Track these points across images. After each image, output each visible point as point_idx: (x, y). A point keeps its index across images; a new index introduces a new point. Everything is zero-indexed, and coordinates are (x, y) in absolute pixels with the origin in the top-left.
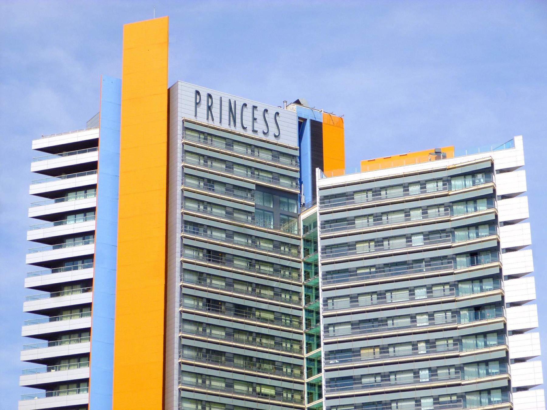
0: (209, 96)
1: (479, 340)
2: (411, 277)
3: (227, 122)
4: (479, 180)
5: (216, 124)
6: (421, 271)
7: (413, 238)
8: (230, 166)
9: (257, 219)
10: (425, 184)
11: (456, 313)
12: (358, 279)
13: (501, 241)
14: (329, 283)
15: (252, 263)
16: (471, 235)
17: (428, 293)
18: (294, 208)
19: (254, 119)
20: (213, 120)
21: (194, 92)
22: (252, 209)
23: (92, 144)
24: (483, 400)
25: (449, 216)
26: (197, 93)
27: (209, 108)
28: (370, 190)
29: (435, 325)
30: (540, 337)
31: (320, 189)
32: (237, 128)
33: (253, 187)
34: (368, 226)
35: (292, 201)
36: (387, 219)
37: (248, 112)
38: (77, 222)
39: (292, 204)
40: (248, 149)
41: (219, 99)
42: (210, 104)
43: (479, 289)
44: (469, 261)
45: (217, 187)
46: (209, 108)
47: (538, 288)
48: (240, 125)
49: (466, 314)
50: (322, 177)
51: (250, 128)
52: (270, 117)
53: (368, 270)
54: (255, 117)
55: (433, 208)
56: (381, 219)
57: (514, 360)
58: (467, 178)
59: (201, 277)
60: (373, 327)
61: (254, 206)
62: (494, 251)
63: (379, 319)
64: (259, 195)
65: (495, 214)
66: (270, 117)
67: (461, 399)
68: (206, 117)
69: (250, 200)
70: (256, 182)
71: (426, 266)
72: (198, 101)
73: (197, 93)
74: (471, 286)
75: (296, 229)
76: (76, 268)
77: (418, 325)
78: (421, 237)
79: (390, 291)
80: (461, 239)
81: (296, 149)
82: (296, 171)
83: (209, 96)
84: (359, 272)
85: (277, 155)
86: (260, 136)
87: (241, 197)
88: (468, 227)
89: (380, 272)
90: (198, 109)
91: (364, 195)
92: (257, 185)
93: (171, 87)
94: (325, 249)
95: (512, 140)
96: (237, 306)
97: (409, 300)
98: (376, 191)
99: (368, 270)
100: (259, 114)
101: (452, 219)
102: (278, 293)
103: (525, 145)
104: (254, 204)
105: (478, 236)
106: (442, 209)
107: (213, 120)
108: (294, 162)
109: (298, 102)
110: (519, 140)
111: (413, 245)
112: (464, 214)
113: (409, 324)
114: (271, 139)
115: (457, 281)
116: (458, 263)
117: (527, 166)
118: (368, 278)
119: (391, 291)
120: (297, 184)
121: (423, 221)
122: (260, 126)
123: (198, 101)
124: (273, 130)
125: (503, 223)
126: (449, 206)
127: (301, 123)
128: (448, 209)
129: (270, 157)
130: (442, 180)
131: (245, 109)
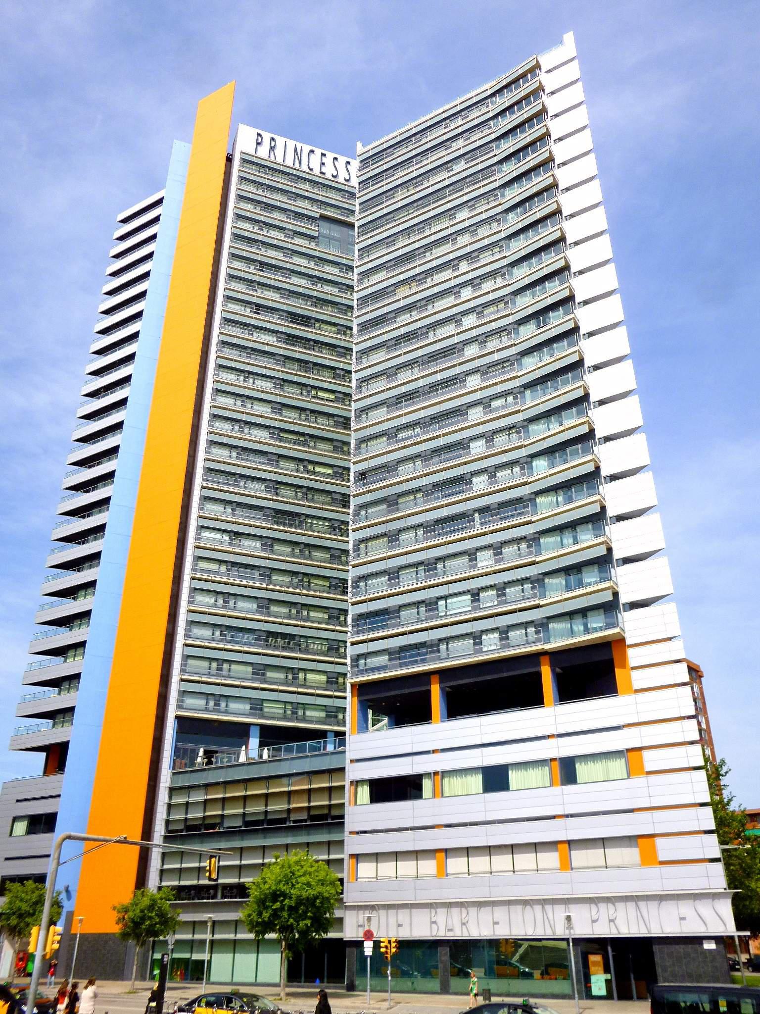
1: (575, 625)
7: (484, 637)
10: (504, 589)
13: (614, 546)
16: (565, 541)
17: (501, 639)
24: (575, 628)
25: (542, 643)
28: (421, 563)
29: (506, 603)
30: (679, 619)
34: (417, 541)
36: (444, 567)
43: (582, 628)
44: (549, 465)
47: (621, 275)
55: (504, 469)
56: (436, 569)
57: (628, 605)
58: (574, 618)
60: (419, 655)
63: (428, 643)
65: (600, 504)
67: (540, 630)
74: (559, 539)
77: (485, 649)
79: (445, 639)
80: (562, 636)
88: (560, 529)
91: (412, 534)
94: (358, 620)
97: (473, 652)
98: (429, 564)
105: (576, 542)
106: (523, 546)
111: (485, 649)
115: (542, 574)
116: (551, 632)
117: (606, 202)
119: (445, 598)
121: (490, 488)
125: (621, 561)
126: (523, 427)
128: (540, 630)
130: (529, 581)
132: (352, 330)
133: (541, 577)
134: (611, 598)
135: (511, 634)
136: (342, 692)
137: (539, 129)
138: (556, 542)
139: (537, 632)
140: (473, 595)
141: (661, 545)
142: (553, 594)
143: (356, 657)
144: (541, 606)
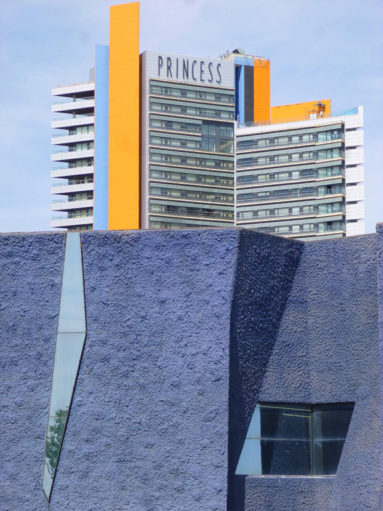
0: (169, 59)
2: (290, 200)
3: (182, 76)
4: (335, 135)
5: (174, 79)
6: (297, 197)
8: (184, 109)
9: (203, 145)
11: (316, 225)
12: (258, 200)
14: (240, 202)
15: (199, 178)
18: (231, 133)
19: (202, 71)
20: (171, 76)
21: (158, 57)
22: (199, 139)
23: (89, 94)
26: (160, 58)
27: (169, 68)
31: (237, 137)
32: (189, 80)
33: (200, 122)
35: (229, 129)
37: (197, 68)
38: (83, 149)
39: (230, 131)
40: (197, 94)
41: (176, 60)
42: (169, 65)
45: (175, 126)
46: (169, 68)
48: (192, 77)
49: (322, 226)
50: (239, 127)
51: (198, 79)
52: (214, 69)
53: (264, 194)
54: (203, 70)
59: (164, 191)
61: (140, 227)
62: (342, 184)
64: (205, 127)
66: (214, 69)
68: (166, 74)
69: (198, 132)
70: (203, 119)
71: (300, 193)
72: (160, 64)
73: (160, 58)
75: (232, 149)
76: (83, 182)
77: (293, 232)
78: (298, 173)
80: (323, 212)
81: (233, 90)
82: (233, 107)
83: (169, 59)
84: (259, 195)
85: (219, 96)
86: (207, 83)
87: (192, 131)
89: (272, 196)
90: (161, 70)
91: (264, 142)
92: (205, 122)
93: (143, 53)
94: (239, 144)
95: (357, 107)
96: (189, 208)
99: (264, 194)
100: (205, 68)
101: (316, 162)
102: (218, 197)
103: (365, 112)
104: (201, 135)
107: (171, 76)
108: (232, 101)
109: (236, 52)
110: (361, 109)
112: (324, 159)
113: (288, 231)
114: (215, 84)
118: (264, 200)
120: (233, 116)
122: (206, 76)
123: (160, 64)
124: (216, 77)
127: (238, 69)
129: (214, 98)
131: (195, 65)
132: (234, 197)
133: (317, 152)
134: (341, 164)
135: (304, 155)
136: (232, 170)
137: (335, 197)
138: (324, 173)
139: (313, 156)
140: (289, 138)
141: (361, 125)
142: (321, 213)
143: (238, 195)
144: (316, 146)
